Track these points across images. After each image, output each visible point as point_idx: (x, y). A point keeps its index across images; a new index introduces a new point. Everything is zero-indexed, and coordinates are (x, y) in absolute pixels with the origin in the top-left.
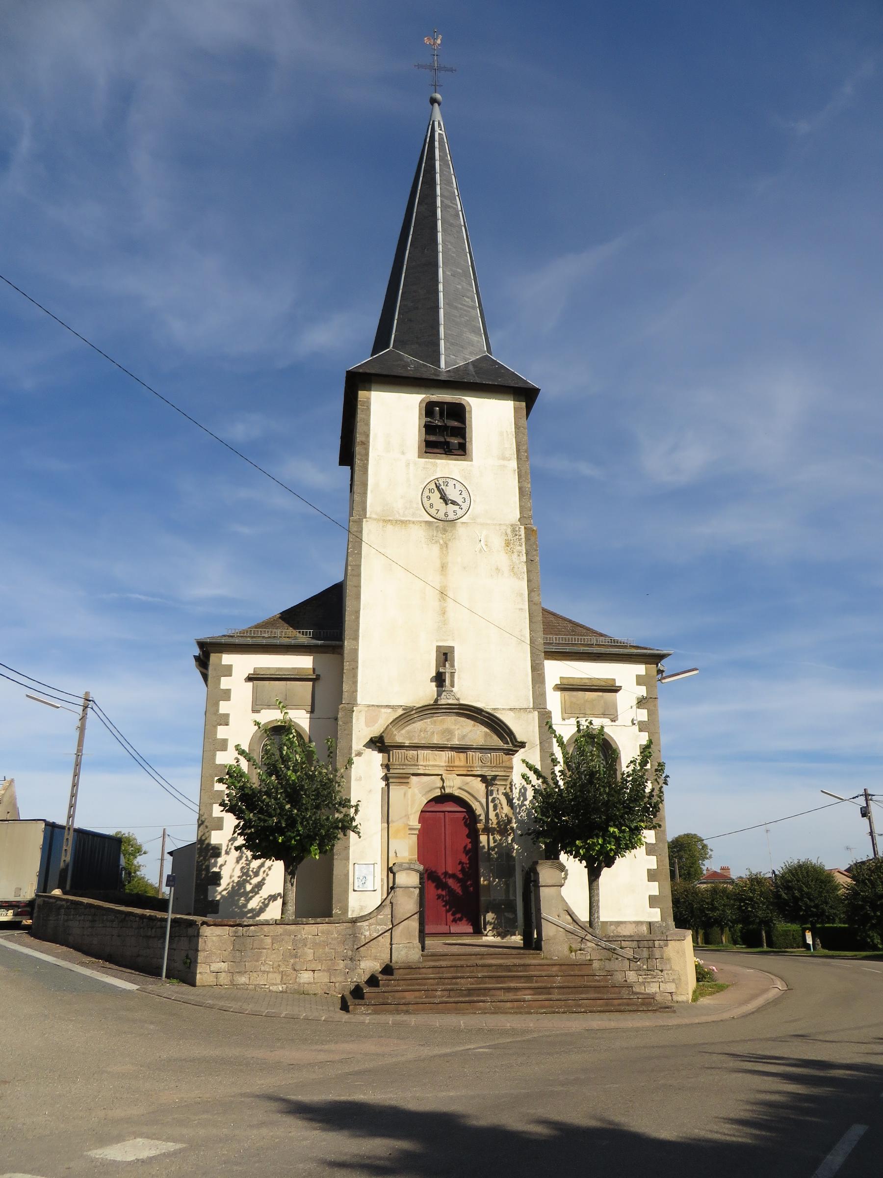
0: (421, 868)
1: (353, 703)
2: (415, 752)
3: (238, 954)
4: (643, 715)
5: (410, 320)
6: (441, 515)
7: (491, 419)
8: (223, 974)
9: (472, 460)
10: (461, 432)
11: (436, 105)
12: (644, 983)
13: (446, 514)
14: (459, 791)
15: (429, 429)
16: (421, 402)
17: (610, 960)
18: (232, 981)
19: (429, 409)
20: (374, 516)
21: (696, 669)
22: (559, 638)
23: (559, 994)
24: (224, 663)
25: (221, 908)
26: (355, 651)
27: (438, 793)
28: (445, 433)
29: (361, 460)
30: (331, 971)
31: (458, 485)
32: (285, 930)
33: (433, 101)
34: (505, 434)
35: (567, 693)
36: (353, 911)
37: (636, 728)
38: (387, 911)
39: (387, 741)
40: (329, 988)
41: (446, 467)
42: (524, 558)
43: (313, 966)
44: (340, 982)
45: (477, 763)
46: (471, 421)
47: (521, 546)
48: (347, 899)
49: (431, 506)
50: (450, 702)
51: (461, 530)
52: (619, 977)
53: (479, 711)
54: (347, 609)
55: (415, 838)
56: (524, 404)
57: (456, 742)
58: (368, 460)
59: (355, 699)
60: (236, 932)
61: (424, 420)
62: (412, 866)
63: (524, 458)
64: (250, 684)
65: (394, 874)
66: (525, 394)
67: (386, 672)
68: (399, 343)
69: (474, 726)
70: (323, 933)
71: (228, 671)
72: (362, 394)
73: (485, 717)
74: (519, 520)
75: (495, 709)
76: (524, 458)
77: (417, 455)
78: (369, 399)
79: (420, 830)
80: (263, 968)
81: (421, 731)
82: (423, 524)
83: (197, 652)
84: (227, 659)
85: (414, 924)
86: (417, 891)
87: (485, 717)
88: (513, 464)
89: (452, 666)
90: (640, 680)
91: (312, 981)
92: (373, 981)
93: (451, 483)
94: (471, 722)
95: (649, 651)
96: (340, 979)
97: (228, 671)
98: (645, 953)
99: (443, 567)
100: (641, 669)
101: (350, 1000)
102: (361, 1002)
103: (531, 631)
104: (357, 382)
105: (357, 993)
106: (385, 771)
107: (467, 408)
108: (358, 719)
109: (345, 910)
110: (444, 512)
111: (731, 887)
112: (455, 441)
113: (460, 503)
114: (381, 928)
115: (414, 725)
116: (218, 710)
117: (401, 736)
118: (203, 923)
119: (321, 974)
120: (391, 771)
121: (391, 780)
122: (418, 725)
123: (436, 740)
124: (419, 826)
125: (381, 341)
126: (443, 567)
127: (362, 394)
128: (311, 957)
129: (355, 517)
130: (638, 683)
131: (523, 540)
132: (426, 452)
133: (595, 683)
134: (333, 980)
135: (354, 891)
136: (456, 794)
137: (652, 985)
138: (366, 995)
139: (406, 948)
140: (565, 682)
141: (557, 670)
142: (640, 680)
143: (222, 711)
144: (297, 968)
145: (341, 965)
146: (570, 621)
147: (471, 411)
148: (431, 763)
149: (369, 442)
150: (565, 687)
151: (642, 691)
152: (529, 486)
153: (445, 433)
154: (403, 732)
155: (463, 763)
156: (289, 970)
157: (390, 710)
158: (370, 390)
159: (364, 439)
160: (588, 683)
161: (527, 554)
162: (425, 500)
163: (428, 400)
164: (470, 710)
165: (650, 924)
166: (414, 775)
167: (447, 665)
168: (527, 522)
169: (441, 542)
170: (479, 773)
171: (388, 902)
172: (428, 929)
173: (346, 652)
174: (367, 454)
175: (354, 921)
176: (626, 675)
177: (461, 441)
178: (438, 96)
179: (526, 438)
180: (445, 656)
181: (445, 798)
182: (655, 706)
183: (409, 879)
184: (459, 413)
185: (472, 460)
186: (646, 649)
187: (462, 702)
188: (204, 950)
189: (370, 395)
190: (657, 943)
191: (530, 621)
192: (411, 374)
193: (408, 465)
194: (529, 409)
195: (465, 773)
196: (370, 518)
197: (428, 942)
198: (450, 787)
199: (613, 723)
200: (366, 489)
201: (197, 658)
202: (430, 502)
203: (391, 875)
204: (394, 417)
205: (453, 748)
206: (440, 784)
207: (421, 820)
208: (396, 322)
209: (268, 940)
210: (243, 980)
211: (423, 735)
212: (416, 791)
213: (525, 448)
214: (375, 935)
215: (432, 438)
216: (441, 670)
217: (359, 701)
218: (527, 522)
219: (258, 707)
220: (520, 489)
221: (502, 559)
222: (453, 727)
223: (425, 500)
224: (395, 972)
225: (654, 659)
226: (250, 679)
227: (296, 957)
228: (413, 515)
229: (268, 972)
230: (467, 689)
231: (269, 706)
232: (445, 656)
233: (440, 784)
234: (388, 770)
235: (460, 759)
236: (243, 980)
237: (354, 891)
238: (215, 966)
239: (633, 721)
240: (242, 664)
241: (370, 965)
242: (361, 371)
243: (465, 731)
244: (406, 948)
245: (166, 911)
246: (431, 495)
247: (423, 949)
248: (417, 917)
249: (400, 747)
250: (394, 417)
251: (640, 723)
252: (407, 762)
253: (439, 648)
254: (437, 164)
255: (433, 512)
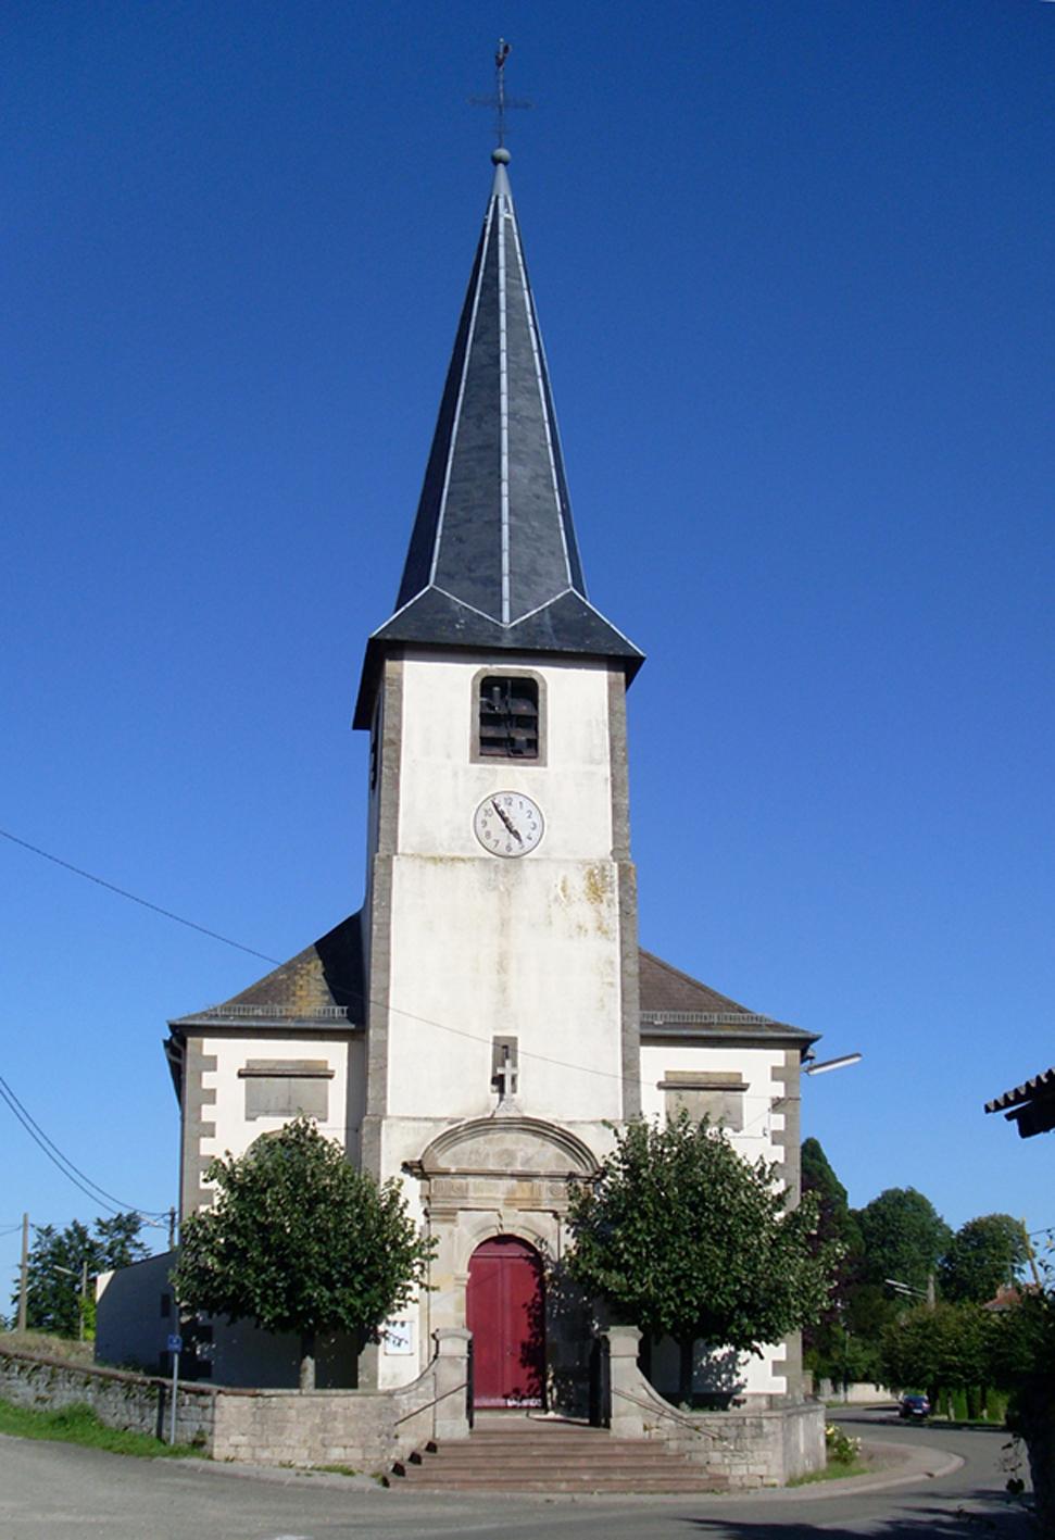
0: (469, 1335)
1: (381, 1114)
2: (463, 1181)
3: (258, 1427)
4: (778, 1122)
5: (460, 540)
6: (502, 849)
7: (575, 699)
8: (244, 1449)
9: (545, 765)
10: (531, 722)
11: (501, 166)
12: (729, 1465)
13: (509, 848)
14: (521, 1230)
15: (487, 718)
16: (474, 678)
17: (691, 1439)
18: (253, 1455)
19: (487, 685)
20: (408, 851)
21: (858, 1055)
22: (667, 1005)
23: (622, 1474)
24: (206, 1052)
25: (214, 1370)
26: (384, 1043)
27: (494, 1233)
28: (509, 725)
29: (390, 768)
30: (364, 1447)
31: (526, 802)
32: (312, 1402)
33: (496, 161)
34: (594, 723)
35: (673, 1093)
36: (384, 1379)
37: (769, 1140)
38: (430, 1383)
39: (427, 1168)
40: (363, 1466)
41: (509, 775)
42: (617, 910)
43: (345, 1441)
44: (377, 1460)
45: (545, 1195)
46: (545, 706)
47: (612, 892)
48: (376, 1363)
49: (488, 834)
50: (511, 1115)
51: (529, 870)
52: (700, 1458)
53: (549, 1127)
54: (373, 985)
55: (464, 1291)
56: (622, 675)
57: (518, 1168)
58: (398, 768)
59: (384, 1109)
60: (256, 1403)
61: (479, 699)
62: (459, 1333)
63: (620, 760)
64: (243, 1081)
65: (438, 1342)
66: (626, 665)
67: (428, 1067)
68: (446, 576)
69: (543, 1145)
70: (354, 1405)
71: (212, 1063)
72: (389, 665)
73: (556, 1133)
74: (612, 853)
75: (570, 1123)
76: (620, 760)
77: (468, 759)
78: (400, 674)
79: (469, 1281)
80: (288, 1442)
81: (471, 1153)
82: (476, 863)
83: (168, 1035)
84: (210, 1046)
85: (461, 1398)
86: (465, 1362)
87: (556, 1133)
88: (606, 770)
89: (515, 1065)
90: (777, 1074)
91: (343, 1457)
92: (415, 1458)
93: (516, 800)
94: (538, 1141)
95: (793, 1035)
96: (377, 1456)
97: (212, 1063)
98: (732, 1432)
99: (504, 924)
100: (778, 1057)
101: (392, 1478)
102: (401, 1478)
103: (623, 1013)
104: (381, 652)
105: (399, 1469)
106: (426, 1205)
107: (541, 686)
108: (388, 1136)
109: (374, 1379)
110: (506, 843)
111: (993, 1325)
112: (521, 736)
113: (523, 838)
114: (423, 1402)
115: (463, 1144)
116: (200, 1118)
117: (444, 1161)
118: (219, 1392)
119: (353, 1450)
120: (433, 1205)
121: (432, 1217)
122: (467, 1146)
123: (492, 1166)
124: (469, 1275)
125: (415, 575)
126: (504, 924)
127: (389, 665)
128: (341, 1432)
129: (382, 853)
130: (774, 1078)
131: (617, 883)
132: (481, 754)
133: (713, 1079)
134: (368, 1457)
135: (386, 1354)
136: (518, 1235)
137: (740, 1467)
138: (407, 1473)
139: (452, 1426)
140: (672, 1078)
141: (658, 1062)
142: (777, 1074)
143: (205, 1118)
144: (326, 1443)
145: (377, 1441)
146: (688, 981)
147: (545, 691)
148: (485, 1195)
149: (400, 741)
150: (671, 1085)
151: (779, 1090)
152: (627, 802)
153: (509, 725)
154: (448, 1153)
155: (527, 1195)
156: (317, 1445)
157: (430, 1124)
158: (402, 659)
159: (392, 736)
160: (704, 1079)
161: (621, 903)
162: (479, 825)
163: (484, 675)
164: (539, 1126)
165: (771, 1396)
166: (462, 1209)
167: (508, 1063)
168: (623, 855)
169: (502, 888)
170: (548, 1208)
171: (430, 1373)
172: (476, 1403)
173: (371, 1044)
174: (398, 759)
175: (390, 1394)
176: (758, 1067)
177: (531, 736)
178: (503, 153)
179: (624, 729)
180: (505, 1050)
181: (503, 1239)
182: (795, 1110)
183: (456, 1348)
184: (528, 690)
185: (545, 765)
186: (793, 1030)
187: (527, 1114)
188: (220, 1421)
189: (402, 665)
190: (748, 1421)
191: (623, 1000)
192: (459, 639)
193: (455, 774)
194: (628, 682)
195: (529, 1207)
196: (403, 855)
197: (477, 1416)
198: (508, 1225)
199: (737, 1134)
200: (397, 812)
201: (167, 1044)
202: (487, 829)
203: (433, 1342)
204: (436, 698)
205: (513, 1176)
206: (496, 1221)
207: (472, 1266)
208: (438, 541)
209: (293, 1413)
210: (266, 1454)
211: (473, 1157)
212: (465, 1231)
213: (622, 744)
214: (415, 1409)
215: (491, 733)
216: (500, 1071)
217: (389, 1112)
218: (623, 855)
219: (252, 1114)
220: (614, 806)
221: (584, 911)
222: (514, 1147)
223: (479, 825)
224: (439, 1449)
225: (802, 1044)
226: (241, 1075)
227: (325, 1431)
228: (463, 848)
229: (294, 1448)
230: (535, 1096)
231: (267, 1113)
232: (505, 1050)
233: (496, 1221)
234: (430, 1203)
235: (523, 1189)
236: (266, 1454)
237: (386, 1354)
238: (234, 1439)
239: (764, 1130)
240: (227, 1056)
241: (409, 1442)
242: (388, 637)
243: (530, 1151)
244: (452, 1426)
245: (171, 1377)
246: (487, 818)
247: (471, 1425)
248: (465, 1389)
249: (446, 1173)
250: (436, 698)
251: (774, 1133)
252: (453, 1194)
253: (496, 1038)
254: (502, 273)
255: (490, 843)
